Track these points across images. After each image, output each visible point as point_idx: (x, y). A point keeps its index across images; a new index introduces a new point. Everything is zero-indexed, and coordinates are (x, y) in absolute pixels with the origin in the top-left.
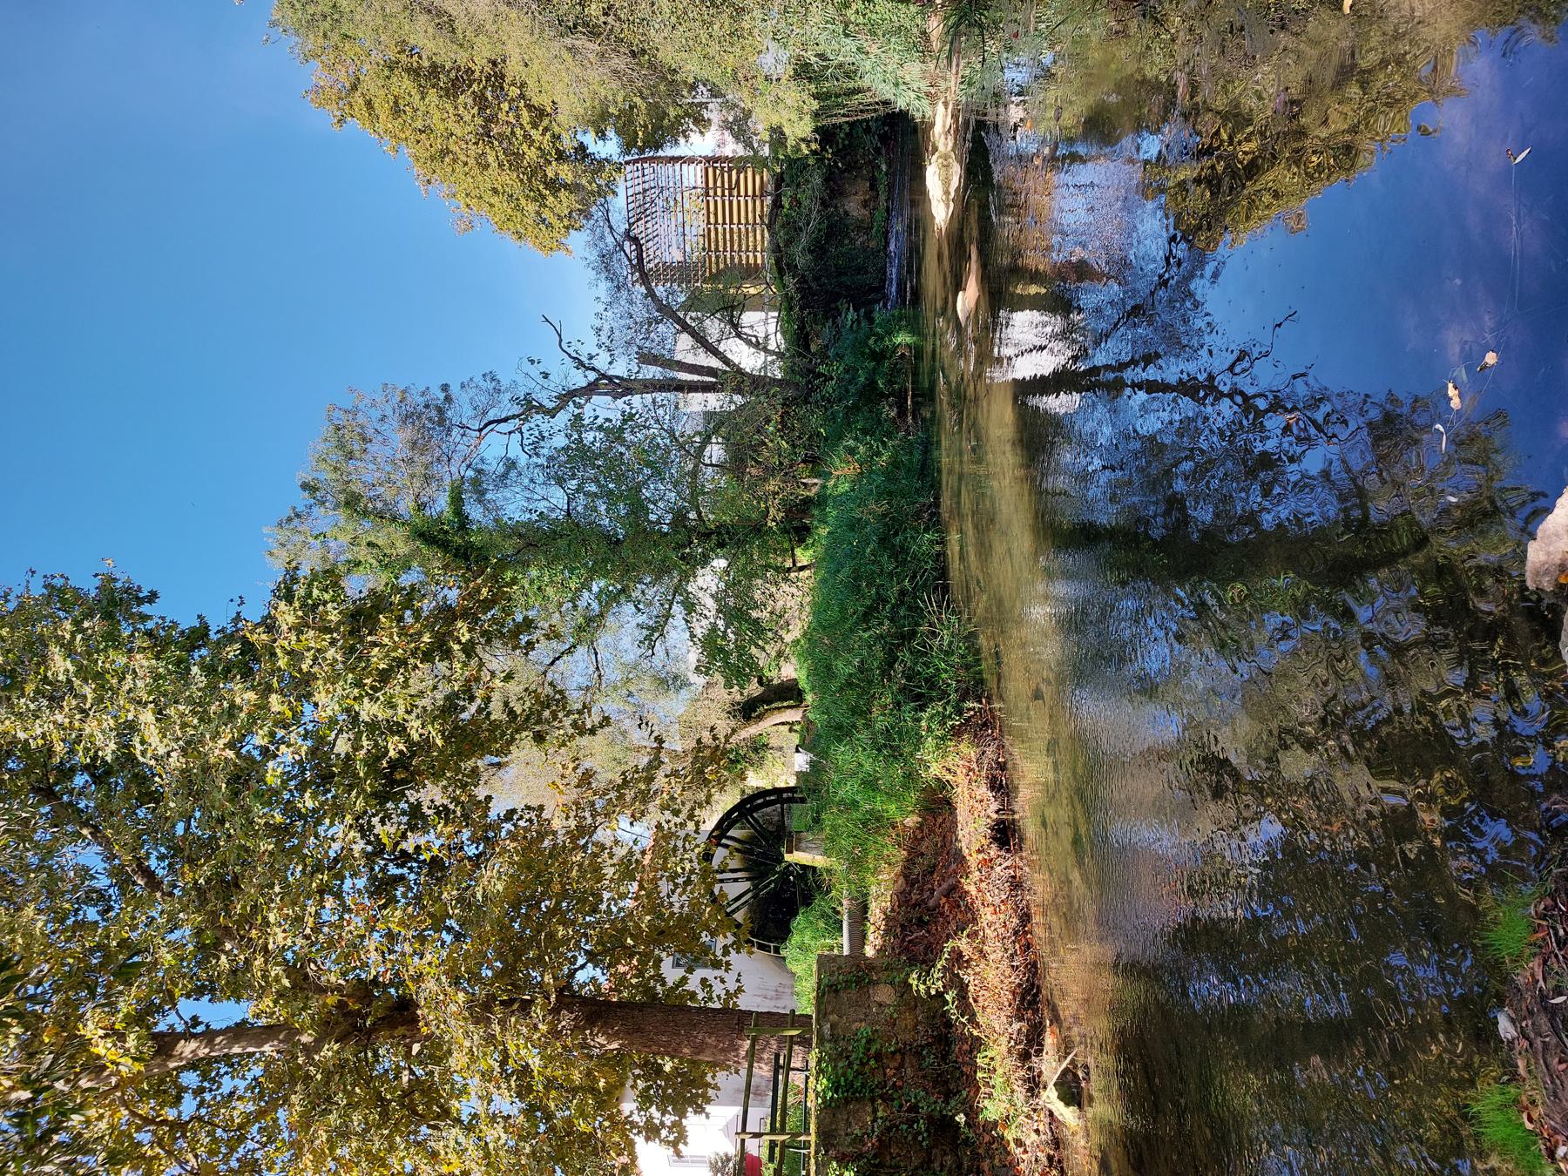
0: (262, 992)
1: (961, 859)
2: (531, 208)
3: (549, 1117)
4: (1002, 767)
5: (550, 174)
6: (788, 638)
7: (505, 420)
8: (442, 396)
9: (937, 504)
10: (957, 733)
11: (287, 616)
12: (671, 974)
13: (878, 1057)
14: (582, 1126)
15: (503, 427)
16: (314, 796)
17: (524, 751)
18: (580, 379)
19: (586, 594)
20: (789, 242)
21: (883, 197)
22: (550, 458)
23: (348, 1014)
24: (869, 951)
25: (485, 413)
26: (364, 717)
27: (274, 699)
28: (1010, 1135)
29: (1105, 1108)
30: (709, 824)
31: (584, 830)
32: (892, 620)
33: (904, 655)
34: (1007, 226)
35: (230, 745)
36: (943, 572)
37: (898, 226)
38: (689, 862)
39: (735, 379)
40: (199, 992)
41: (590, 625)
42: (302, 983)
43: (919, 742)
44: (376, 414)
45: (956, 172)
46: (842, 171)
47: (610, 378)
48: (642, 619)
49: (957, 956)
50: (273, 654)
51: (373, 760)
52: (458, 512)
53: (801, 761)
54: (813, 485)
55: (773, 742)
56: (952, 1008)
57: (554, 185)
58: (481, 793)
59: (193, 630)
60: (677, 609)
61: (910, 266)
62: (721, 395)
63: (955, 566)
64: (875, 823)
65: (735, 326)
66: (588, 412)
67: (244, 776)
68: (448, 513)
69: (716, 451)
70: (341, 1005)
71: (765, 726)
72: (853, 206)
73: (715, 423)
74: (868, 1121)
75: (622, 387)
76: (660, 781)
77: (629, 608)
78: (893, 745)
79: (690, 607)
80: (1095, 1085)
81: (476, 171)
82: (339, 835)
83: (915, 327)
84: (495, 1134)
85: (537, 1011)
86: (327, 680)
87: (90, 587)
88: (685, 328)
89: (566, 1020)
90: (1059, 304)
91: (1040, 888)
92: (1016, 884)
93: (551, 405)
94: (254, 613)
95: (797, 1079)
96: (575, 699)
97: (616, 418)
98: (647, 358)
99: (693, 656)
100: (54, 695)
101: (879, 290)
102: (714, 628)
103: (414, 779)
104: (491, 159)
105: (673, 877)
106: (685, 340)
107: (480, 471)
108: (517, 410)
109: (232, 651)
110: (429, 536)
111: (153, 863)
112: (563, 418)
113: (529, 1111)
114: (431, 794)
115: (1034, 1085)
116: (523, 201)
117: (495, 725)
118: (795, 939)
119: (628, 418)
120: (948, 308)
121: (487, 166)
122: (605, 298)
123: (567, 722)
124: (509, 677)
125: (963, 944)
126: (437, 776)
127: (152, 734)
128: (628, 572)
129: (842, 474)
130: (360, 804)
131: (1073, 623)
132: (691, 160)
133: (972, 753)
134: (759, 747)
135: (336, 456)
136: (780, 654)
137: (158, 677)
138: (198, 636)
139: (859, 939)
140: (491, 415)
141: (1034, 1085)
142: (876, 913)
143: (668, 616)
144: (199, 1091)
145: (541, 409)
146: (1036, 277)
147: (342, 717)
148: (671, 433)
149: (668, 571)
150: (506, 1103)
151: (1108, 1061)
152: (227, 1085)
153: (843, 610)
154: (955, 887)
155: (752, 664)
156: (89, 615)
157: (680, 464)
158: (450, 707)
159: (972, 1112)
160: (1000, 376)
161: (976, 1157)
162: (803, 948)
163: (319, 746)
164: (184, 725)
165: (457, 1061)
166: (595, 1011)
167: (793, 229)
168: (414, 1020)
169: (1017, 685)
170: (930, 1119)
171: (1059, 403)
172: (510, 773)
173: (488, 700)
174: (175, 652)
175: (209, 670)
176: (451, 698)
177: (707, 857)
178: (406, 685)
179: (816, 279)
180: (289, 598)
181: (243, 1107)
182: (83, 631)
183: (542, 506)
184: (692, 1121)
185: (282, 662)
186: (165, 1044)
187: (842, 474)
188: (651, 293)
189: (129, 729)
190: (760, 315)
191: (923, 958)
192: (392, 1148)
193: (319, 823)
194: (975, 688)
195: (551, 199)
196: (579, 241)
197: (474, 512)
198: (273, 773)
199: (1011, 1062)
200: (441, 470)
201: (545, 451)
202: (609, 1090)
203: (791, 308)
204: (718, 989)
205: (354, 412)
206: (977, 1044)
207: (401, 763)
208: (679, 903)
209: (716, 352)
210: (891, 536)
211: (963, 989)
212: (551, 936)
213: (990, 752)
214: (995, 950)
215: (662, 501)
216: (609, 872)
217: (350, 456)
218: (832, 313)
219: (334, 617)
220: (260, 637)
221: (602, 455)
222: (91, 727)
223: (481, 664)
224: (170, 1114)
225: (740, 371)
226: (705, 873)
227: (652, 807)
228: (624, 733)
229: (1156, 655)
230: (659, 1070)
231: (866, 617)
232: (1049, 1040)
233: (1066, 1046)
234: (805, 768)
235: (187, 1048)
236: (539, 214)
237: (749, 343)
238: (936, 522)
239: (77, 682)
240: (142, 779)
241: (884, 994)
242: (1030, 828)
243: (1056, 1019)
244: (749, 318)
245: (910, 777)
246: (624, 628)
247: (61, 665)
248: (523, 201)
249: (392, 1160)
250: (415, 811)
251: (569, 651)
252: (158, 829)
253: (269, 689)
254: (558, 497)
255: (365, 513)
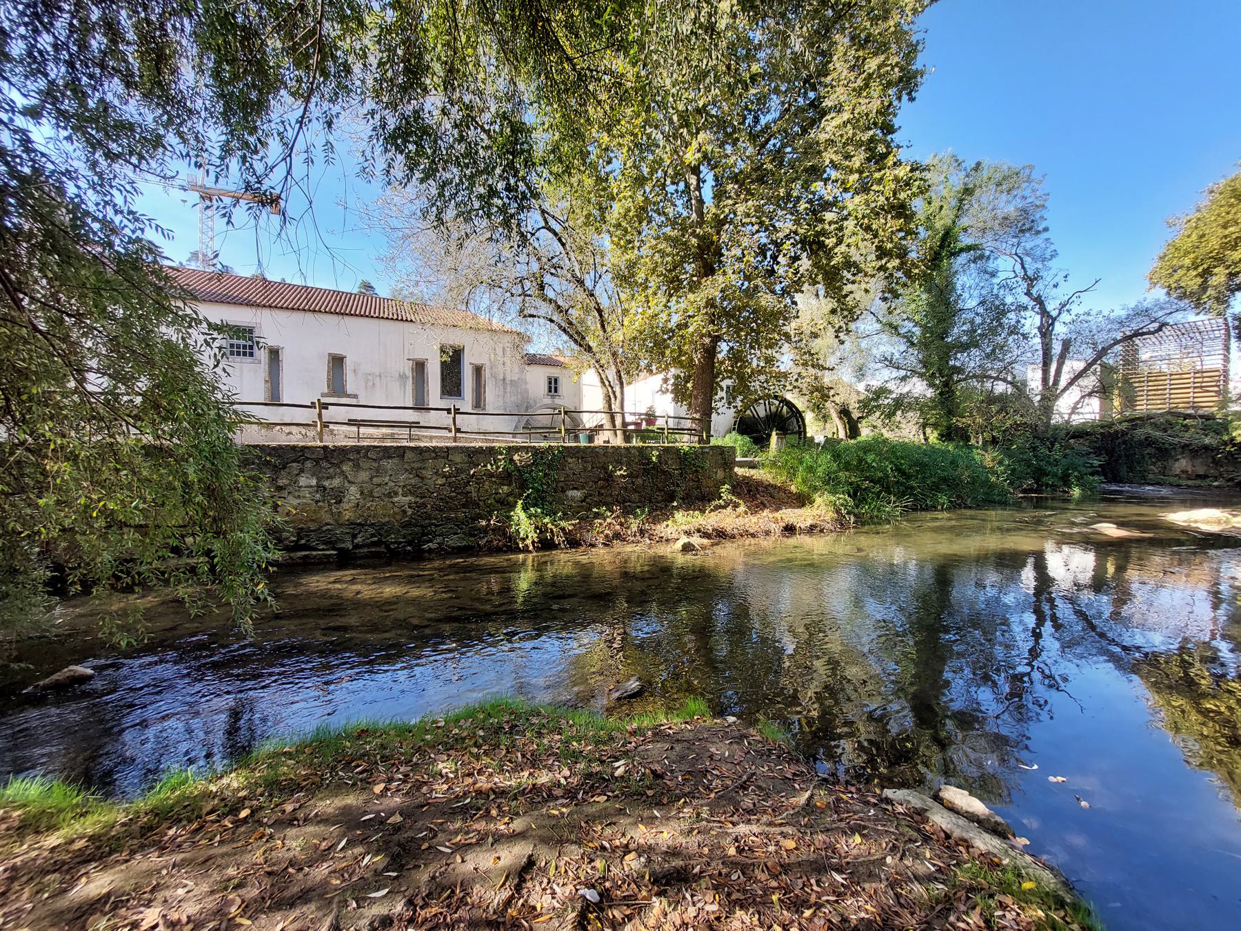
0: (717, 206)
1: (777, 510)
2: (1187, 262)
3: (670, 338)
4: (821, 531)
5: (1216, 270)
6: (884, 431)
7: (1023, 267)
8: (1040, 228)
9: (967, 507)
10: (838, 511)
11: (902, 172)
12: (724, 384)
13: (697, 471)
14: (668, 352)
15: (1018, 267)
16: (806, 209)
17: (828, 304)
18: (1052, 307)
19: (912, 325)
20: (1155, 426)
21: (1190, 483)
22: (997, 296)
23: (708, 248)
24: (736, 469)
25: (1028, 255)
26: (846, 223)
27: (856, 176)
28: (669, 522)
29: (681, 560)
30: (789, 396)
31: (787, 337)
32: (897, 482)
33: (878, 488)
34: (1158, 559)
35: (832, 161)
36: (927, 509)
37: (1165, 491)
38: (773, 388)
39: (1050, 394)
40: (716, 179)
41: (894, 328)
42: (719, 223)
43: (834, 493)
44: (1027, 193)
45: (1215, 529)
46: (1213, 458)
47: (1053, 324)
48: (897, 355)
49: (736, 506)
50: (880, 170)
51: (823, 233)
52: (962, 250)
53: (820, 439)
54: (977, 440)
55: (828, 425)
56: (717, 502)
57: (1207, 273)
58: (806, 287)
59: (892, 126)
60: (902, 373)
61: (1132, 498)
62: (1040, 388)
63: (929, 515)
64: (792, 474)
65: (1090, 395)
66: (1028, 313)
67: (816, 172)
68: (960, 245)
69: (1000, 388)
70: (712, 243)
71: (837, 421)
72: (1182, 464)
73: (1020, 387)
74: (673, 467)
75: (1046, 332)
76: (812, 371)
77: (903, 348)
78: (831, 482)
79: (904, 379)
80: (689, 557)
81: (1221, 221)
82: (785, 225)
83: (1083, 500)
84: (664, 316)
85: (711, 327)
86: (867, 201)
87: (917, 65)
88: (1089, 365)
89: (707, 340)
90: (1098, 584)
91: (766, 543)
92: (768, 533)
93: (1034, 291)
94: (902, 155)
95: (686, 438)
96: (852, 326)
97: (1026, 329)
98: (1066, 344)
99: (876, 383)
100: (857, 66)
101: (1116, 479)
102: (891, 392)
103: (813, 254)
104: (1232, 229)
105: (767, 381)
106: (1080, 366)
107: (988, 258)
108: (1030, 273)
109: (881, 149)
110: (947, 236)
111: (772, 142)
112: (1025, 300)
113: (672, 330)
114: (805, 264)
115: (688, 533)
116: (1192, 256)
117: (840, 289)
118: (739, 437)
119: (1025, 336)
120: (1103, 518)
121: (1225, 227)
122: (1112, 316)
123: (842, 324)
124: (867, 291)
125: (742, 508)
126: (815, 265)
127: (838, 121)
128: (924, 345)
129: (988, 458)
130: (801, 231)
131: (892, 570)
132: (1227, 360)
133: (828, 518)
134: (825, 418)
135: (998, 176)
136: (875, 427)
137: (867, 115)
138: (888, 129)
139: (741, 465)
140: (1027, 260)
141: (688, 533)
142: (753, 472)
143: (898, 368)
144: (677, 191)
145: (1031, 286)
146: (1121, 569)
147: (845, 212)
148: (1015, 362)
149: (925, 366)
150: (676, 319)
151: (698, 562)
152: (679, 203)
153: (902, 458)
154: (765, 506)
155: (870, 413)
156: (902, 70)
157: (993, 367)
158: (849, 264)
159: (677, 508)
160: (1049, 546)
161: (661, 509)
162: (736, 441)
163: (827, 205)
164: (842, 136)
165: (691, 296)
166: (710, 352)
167: (1167, 426)
168: (707, 276)
169: (863, 541)
170: (674, 491)
171: (1028, 575)
172: (814, 301)
173: (854, 282)
174: (880, 120)
175: (871, 140)
176: (855, 265)
177: (776, 397)
178: (863, 240)
179: (1125, 442)
180: (912, 170)
181: (670, 211)
182: (892, 69)
183: (966, 295)
184: (670, 396)
185: (877, 175)
186: (696, 170)
187: (988, 458)
188: (1116, 342)
189: (839, 109)
190: (1097, 409)
191: (734, 491)
192: (658, 276)
193: (792, 214)
194: (861, 521)
195: (1195, 273)
196: (1160, 294)
197: (963, 258)
198: (817, 186)
199: (697, 526)
200: (989, 235)
201: (1002, 292)
202: (681, 363)
203: (1102, 427)
204: (720, 404)
205: (1029, 180)
206: (703, 512)
207: (822, 245)
208: (755, 385)
209: (1071, 384)
210: (949, 483)
211: (724, 507)
212: (742, 330)
213: (829, 526)
214: (740, 522)
215: (970, 361)
216: (770, 352)
217: (999, 184)
218: (1098, 451)
219: (902, 196)
220: (890, 161)
221: (1001, 325)
222: (840, 90)
223: (873, 276)
224: (669, 181)
225: (1057, 397)
226: (769, 396)
227: (800, 369)
228: (833, 353)
229: (875, 610)
230: (687, 382)
231: (899, 470)
232: (705, 541)
233: (703, 548)
234: (816, 441)
235: (693, 180)
236: (1181, 267)
237: (1078, 403)
238: (953, 507)
239: (863, 76)
240: (813, 122)
241: (720, 474)
242: (792, 541)
243: (712, 545)
244: (1095, 404)
245: (815, 489)
246: (893, 347)
247: (872, 64)
248: (1192, 256)
249: (654, 277)
250: (796, 258)
251: (878, 321)
252: (789, 139)
253: (860, 172)
254: (971, 303)
255: (961, 200)
